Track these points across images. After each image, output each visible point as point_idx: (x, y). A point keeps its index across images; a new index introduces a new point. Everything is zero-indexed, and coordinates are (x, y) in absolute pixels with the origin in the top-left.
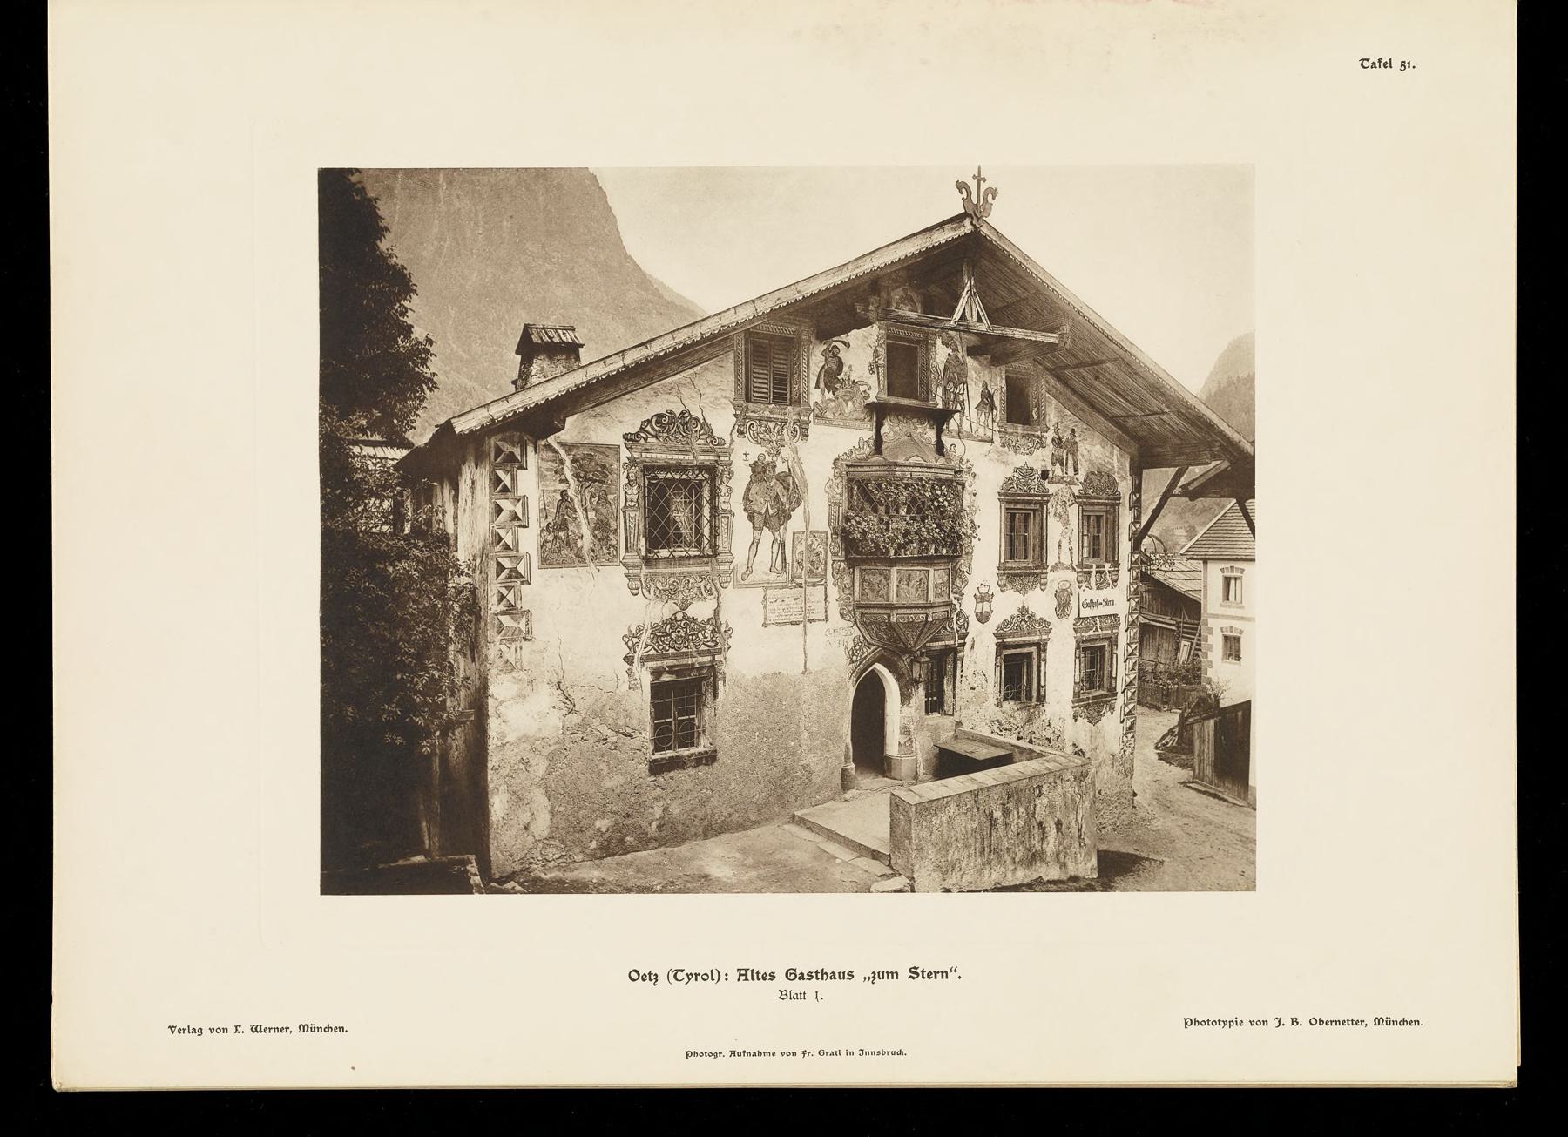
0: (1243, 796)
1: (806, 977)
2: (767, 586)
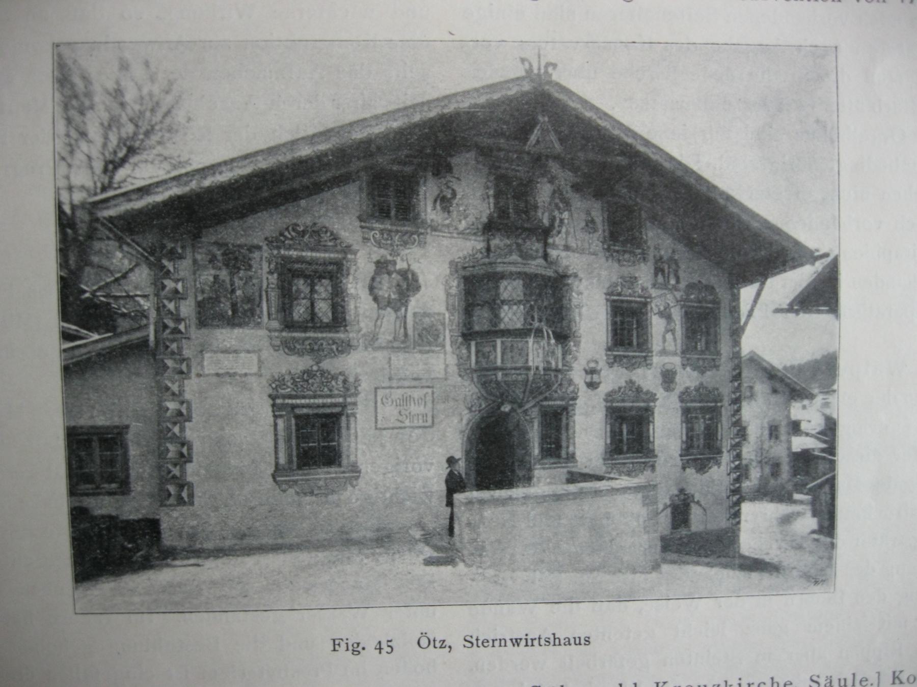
0: (516, 114)
1: (583, 641)
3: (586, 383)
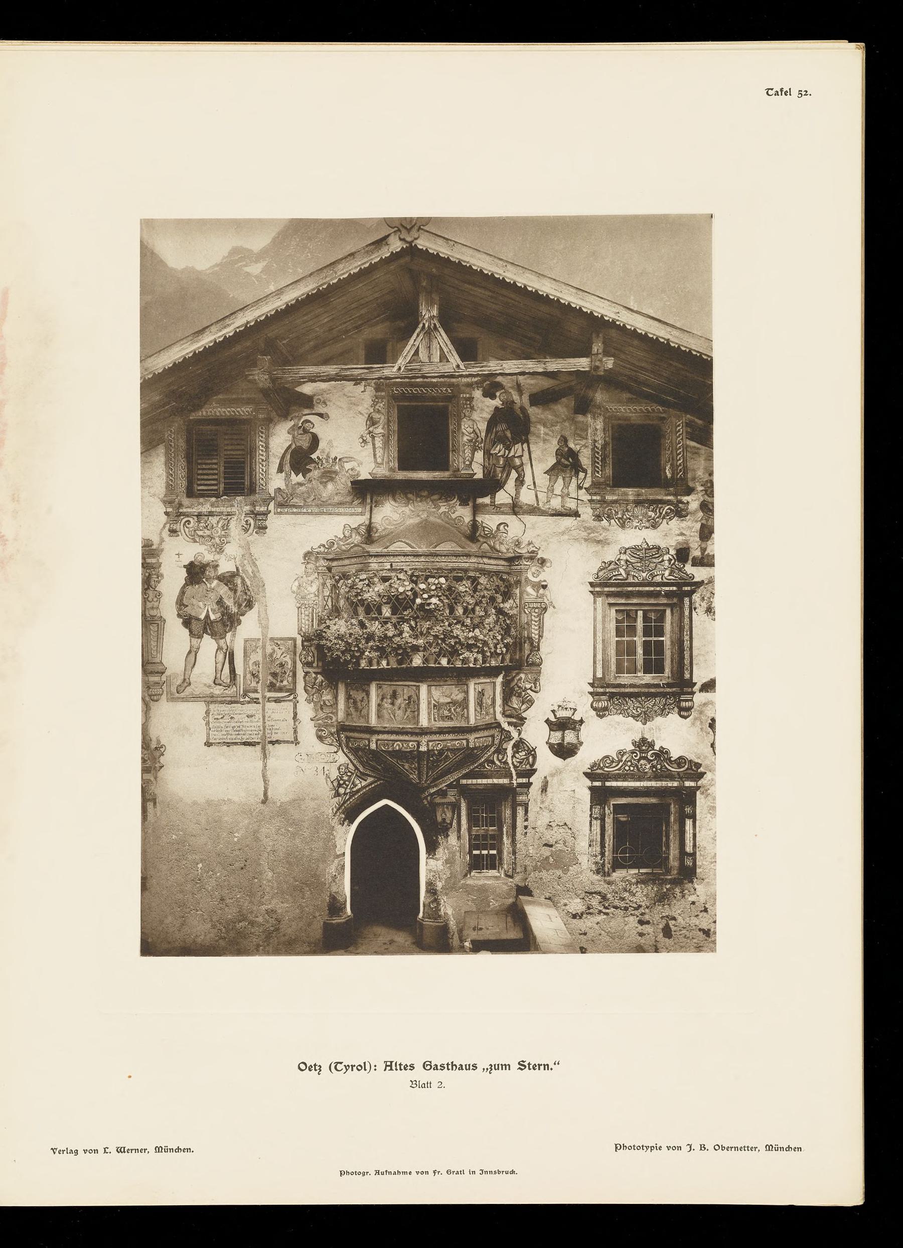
1: (439, 1068)
2: (211, 700)
3: (551, 747)
